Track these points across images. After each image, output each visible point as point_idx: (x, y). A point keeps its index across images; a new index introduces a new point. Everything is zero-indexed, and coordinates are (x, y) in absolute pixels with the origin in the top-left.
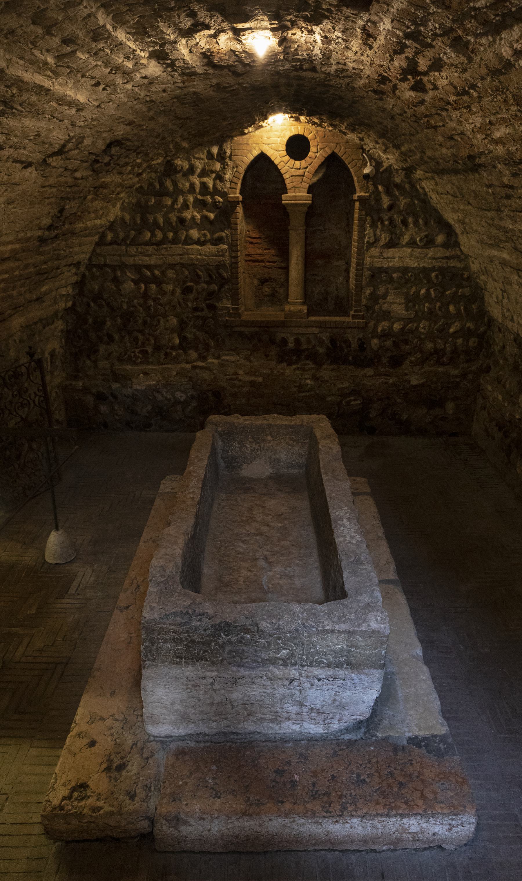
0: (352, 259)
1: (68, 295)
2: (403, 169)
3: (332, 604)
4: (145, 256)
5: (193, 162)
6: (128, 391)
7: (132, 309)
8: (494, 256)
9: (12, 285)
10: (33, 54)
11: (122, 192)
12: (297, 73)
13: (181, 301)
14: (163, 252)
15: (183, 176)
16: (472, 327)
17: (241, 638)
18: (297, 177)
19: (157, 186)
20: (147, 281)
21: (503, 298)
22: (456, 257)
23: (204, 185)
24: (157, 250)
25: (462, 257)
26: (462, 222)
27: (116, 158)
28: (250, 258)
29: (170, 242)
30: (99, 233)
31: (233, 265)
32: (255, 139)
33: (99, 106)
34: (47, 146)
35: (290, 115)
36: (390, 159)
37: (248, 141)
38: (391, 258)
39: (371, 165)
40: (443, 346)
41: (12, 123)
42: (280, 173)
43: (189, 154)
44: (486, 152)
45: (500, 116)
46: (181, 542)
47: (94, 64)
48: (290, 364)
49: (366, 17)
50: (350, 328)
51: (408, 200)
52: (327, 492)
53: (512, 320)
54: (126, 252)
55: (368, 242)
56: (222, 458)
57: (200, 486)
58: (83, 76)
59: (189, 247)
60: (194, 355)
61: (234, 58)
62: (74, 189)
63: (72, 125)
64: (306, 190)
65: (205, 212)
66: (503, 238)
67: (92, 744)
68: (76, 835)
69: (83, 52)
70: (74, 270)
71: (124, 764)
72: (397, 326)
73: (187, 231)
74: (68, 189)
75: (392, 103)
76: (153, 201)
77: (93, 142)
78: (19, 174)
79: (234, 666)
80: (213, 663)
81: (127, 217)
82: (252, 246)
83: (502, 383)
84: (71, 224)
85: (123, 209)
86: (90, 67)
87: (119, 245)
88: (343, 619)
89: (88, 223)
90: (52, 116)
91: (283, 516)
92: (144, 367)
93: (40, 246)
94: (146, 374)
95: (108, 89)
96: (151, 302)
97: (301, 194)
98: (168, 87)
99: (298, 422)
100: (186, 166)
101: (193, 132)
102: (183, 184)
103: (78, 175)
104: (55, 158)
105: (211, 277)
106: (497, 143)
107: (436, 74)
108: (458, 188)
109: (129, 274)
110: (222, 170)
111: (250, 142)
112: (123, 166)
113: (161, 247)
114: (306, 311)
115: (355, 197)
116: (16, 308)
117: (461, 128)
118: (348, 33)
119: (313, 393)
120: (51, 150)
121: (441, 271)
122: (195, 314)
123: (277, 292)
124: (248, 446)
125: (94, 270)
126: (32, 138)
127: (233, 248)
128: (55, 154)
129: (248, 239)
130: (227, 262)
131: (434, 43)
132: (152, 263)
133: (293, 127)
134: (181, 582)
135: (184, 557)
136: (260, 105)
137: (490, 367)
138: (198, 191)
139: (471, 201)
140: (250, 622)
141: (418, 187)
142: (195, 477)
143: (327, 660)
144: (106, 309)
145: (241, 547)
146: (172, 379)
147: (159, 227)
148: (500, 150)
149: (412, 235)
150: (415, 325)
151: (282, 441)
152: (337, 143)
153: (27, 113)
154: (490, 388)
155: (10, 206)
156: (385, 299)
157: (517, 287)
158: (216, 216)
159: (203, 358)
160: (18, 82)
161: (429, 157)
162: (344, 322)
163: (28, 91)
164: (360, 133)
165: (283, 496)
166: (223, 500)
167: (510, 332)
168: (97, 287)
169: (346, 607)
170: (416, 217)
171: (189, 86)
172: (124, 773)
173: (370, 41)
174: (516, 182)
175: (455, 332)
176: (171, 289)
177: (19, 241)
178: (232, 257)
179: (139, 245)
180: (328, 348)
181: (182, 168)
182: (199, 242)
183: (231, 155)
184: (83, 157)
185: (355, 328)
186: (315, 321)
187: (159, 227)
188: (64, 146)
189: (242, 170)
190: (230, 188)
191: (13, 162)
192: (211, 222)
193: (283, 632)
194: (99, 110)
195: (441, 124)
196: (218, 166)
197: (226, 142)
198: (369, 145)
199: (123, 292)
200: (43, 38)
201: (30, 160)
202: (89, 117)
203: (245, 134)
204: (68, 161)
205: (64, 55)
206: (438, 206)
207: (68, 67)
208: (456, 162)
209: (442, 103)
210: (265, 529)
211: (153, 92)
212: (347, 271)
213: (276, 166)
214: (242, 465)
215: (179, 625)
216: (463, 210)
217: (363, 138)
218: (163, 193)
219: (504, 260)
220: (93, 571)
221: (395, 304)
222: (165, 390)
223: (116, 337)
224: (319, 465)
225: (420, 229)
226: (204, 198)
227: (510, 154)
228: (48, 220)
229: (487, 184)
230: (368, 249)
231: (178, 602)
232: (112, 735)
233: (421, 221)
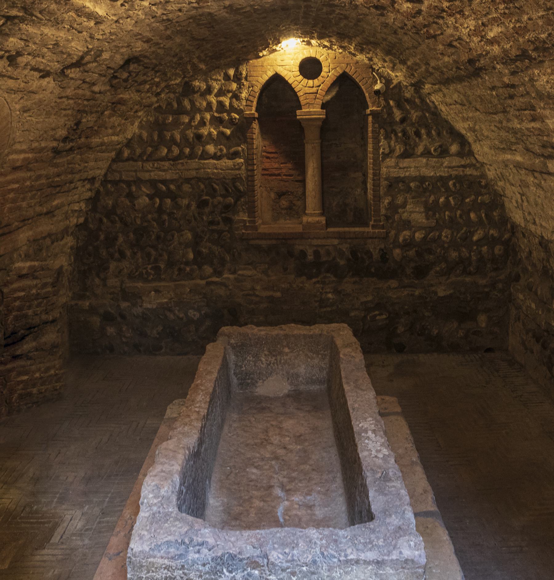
0: (369, 171)
1: (81, 211)
2: (412, 85)
3: (357, 529)
4: (161, 171)
5: (210, 83)
6: (137, 311)
7: (145, 224)
8: (508, 160)
9: (22, 196)
11: (140, 111)
13: (196, 215)
14: (179, 166)
15: (201, 95)
16: (496, 235)
17: (248, 574)
19: (175, 105)
20: (162, 196)
21: (523, 201)
23: (221, 104)
24: (173, 165)
25: (478, 165)
26: (472, 130)
27: (134, 75)
28: (267, 172)
29: (186, 157)
30: (115, 149)
31: (250, 179)
32: (269, 62)
33: (117, 21)
34: (65, 56)
35: (302, 40)
36: (398, 76)
37: (263, 63)
38: (407, 168)
39: (381, 82)
40: (468, 255)
41: (31, 30)
42: (292, 87)
43: (206, 75)
44: (484, 53)
45: (490, 16)
48: (310, 277)
50: (371, 238)
51: (419, 113)
52: (349, 403)
53: (535, 223)
54: (142, 167)
55: (383, 153)
56: (234, 373)
57: (208, 400)
59: (205, 161)
60: (208, 270)
62: (92, 103)
63: (90, 37)
64: (320, 106)
65: (221, 129)
66: (513, 140)
70: (88, 186)
72: (418, 236)
74: (85, 102)
75: (393, 17)
76: (171, 119)
77: (111, 57)
81: (145, 135)
82: (269, 160)
83: (533, 290)
84: (87, 138)
85: (141, 127)
87: (136, 161)
88: (369, 545)
89: (105, 138)
90: (71, 26)
91: (302, 438)
92: (154, 284)
93: (54, 158)
94: (157, 291)
95: (126, 4)
96: (165, 217)
97: (315, 110)
98: (184, 7)
99: (317, 331)
100: (204, 86)
101: (210, 54)
102: (200, 103)
103: (96, 89)
104: (73, 70)
105: (227, 190)
106: (492, 43)
108: (464, 96)
110: (239, 89)
111: (265, 64)
112: (141, 84)
113: (177, 162)
114: (324, 222)
115: (368, 111)
116: (24, 220)
117: (458, 34)
120: (69, 61)
121: (459, 179)
122: (210, 228)
123: (294, 205)
124: (263, 359)
125: (109, 186)
126: (51, 46)
127: (249, 161)
129: (264, 154)
130: (244, 176)
132: (168, 177)
133: (305, 51)
134: (177, 504)
135: (184, 475)
136: (271, 29)
137: (519, 276)
138: (214, 109)
139: (478, 107)
140: (258, 552)
141: (428, 101)
142: (202, 391)
144: (118, 225)
145: (253, 473)
146: (185, 296)
147: (176, 143)
148: (496, 49)
149: (426, 145)
150: (437, 234)
151: (301, 352)
152: (347, 64)
153: (46, 22)
154: (521, 296)
155: (25, 114)
156: (405, 207)
157: (535, 189)
158: (232, 132)
159: (218, 273)
161: (433, 68)
162: (364, 232)
164: (369, 53)
165: (302, 415)
166: (235, 421)
167: (534, 236)
168: (111, 203)
169: (373, 531)
170: (428, 127)
171: (203, 7)
174: (516, 80)
175: (479, 240)
176: (187, 203)
177: (32, 150)
178: (248, 170)
179: (155, 160)
181: (200, 88)
184: (101, 71)
185: (376, 238)
186: (334, 232)
187: (176, 143)
188: (82, 58)
189: (257, 89)
190: (246, 106)
191: (31, 70)
192: (228, 138)
193: (297, 565)
194: (117, 24)
195: (439, 32)
196: (234, 86)
197: (242, 64)
198: (378, 64)
199: (137, 207)
201: (48, 68)
202: (107, 31)
204: (86, 74)
206: (449, 118)
208: (458, 68)
209: (437, 11)
210: (281, 452)
211: (169, 10)
212: (365, 182)
214: (257, 382)
215: (172, 558)
217: (372, 58)
218: (181, 111)
220: (83, 514)
221: (414, 212)
222: (177, 308)
223: (128, 253)
224: (341, 376)
225: (433, 140)
226: (221, 115)
227: (505, 51)
228: (63, 132)
229: (490, 86)
231: (173, 529)
233: (433, 132)
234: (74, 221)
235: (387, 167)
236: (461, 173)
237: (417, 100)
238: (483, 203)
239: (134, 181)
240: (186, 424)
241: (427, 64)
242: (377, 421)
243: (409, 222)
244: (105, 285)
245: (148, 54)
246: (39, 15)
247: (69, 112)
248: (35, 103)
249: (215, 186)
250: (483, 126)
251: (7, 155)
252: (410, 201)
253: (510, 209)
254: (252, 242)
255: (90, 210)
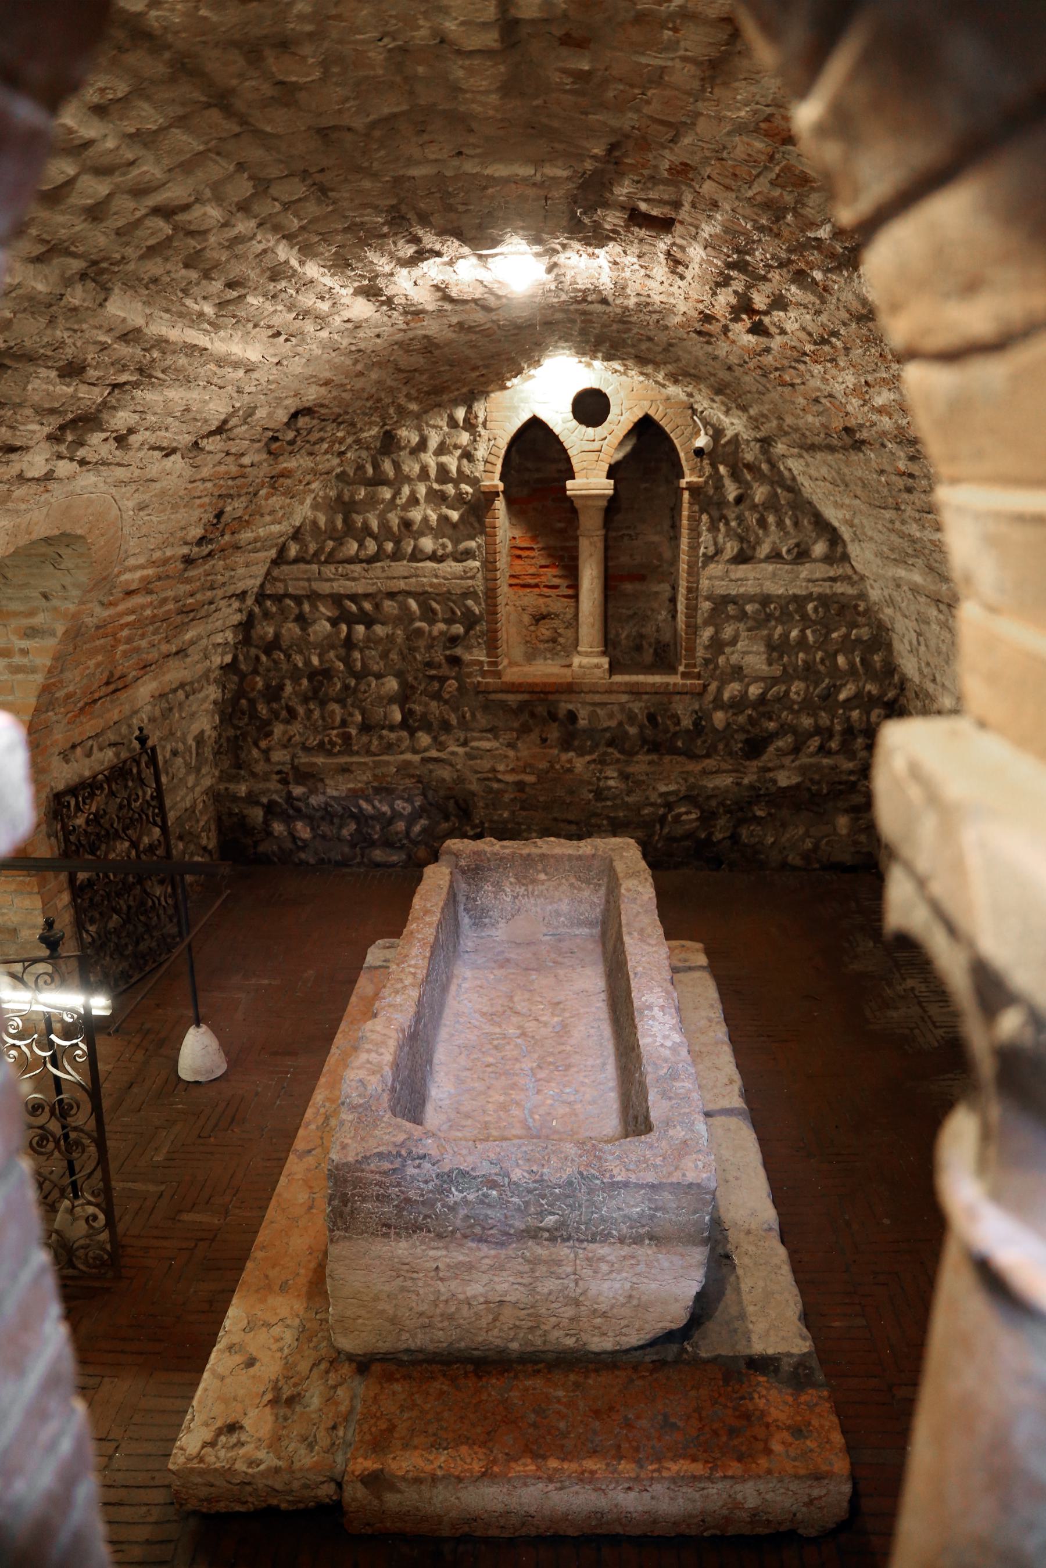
2: (757, 440)
7: (327, 665)
9: (140, 632)
10: (184, 305)
12: (580, 307)
13: (406, 651)
16: (875, 692)
18: (591, 461)
19: (370, 471)
20: (351, 620)
21: (919, 644)
22: (846, 579)
23: (442, 469)
25: (855, 578)
28: (516, 581)
29: (388, 557)
36: (734, 425)
38: (741, 580)
40: (828, 723)
43: (419, 419)
46: (392, 1044)
47: (272, 309)
49: (669, 240)
52: (630, 964)
53: (934, 680)
55: (704, 554)
58: (255, 326)
59: (419, 565)
60: (424, 739)
61: (481, 290)
62: (238, 482)
65: (445, 510)
66: (910, 551)
67: (251, 1362)
68: (222, 1504)
69: (255, 296)
70: (236, 605)
71: (299, 1394)
72: (754, 691)
73: (416, 539)
74: (230, 482)
78: (157, 464)
79: (473, 1240)
80: (440, 1236)
81: (322, 520)
84: (233, 533)
85: (315, 507)
86: (266, 313)
87: (308, 562)
93: (185, 570)
100: (415, 439)
103: (246, 460)
104: (211, 439)
107: (782, 314)
108: (839, 473)
109: (322, 609)
112: (315, 444)
114: (607, 666)
115: (683, 483)
116: (145, 667)
117: (828, 389)
118: (646, 258)
119: (618, 801)
120: (206, 429)
121: (824, 600)
123: (560, 635)
125: (269, 603)
127: (489, 565)
128: (211, 434)
131: (770, 276)
135: (396, 1066)
141: (782, 468)
143: (619, 1231)
147: (371, 534)
149: (774, 543)
150: (783, 688)
158: (461, 517)
160: (161, 343)
162: (668, 684)
163: (174, 352)
172: (298, 1409)
173: (680, 269)
175: (848, 700)
177: (153, 563)
178: (486, 579)
180: (642, 727)
182: (434, 557)
183: (486, 420)
187: (371, 534)
188: (225, 422)
189: (503, 443)
192: (454, 526)
196: (465, 438)
198: (702, 403)
200: (198, 284)
201: (174, 444)
203: (506, 388)
205: (229, 302)
207: (234, 317)
212: (673, 600)
213: (556, 437)
216: (849, 506)
218: (380, 480)
219: (916, 584)
223: (301, 710)
225: (787, 533)
226: (444, 487)
230: (704, 567)
232: (281, 1350)
233: (788, 522)
234: (217, 660)
235: (710, 578)
236: (828, 591)
237: (764, 466)
238: (859, 640)
239: (308, 597)
240: (397, 992)
241: (780, 418)
242: (667, 992)
243: (741, 668)
244: (268, 760)
245: (326, 402)
246: (161, 376)
247: (206, 500)
248: (155, 496)
249: (434, 605)
250: (865, 521)
251: (117, 576)
252: (744, 634)
253: (899, 653)
254: (492, 697)
255: (239, 643)
